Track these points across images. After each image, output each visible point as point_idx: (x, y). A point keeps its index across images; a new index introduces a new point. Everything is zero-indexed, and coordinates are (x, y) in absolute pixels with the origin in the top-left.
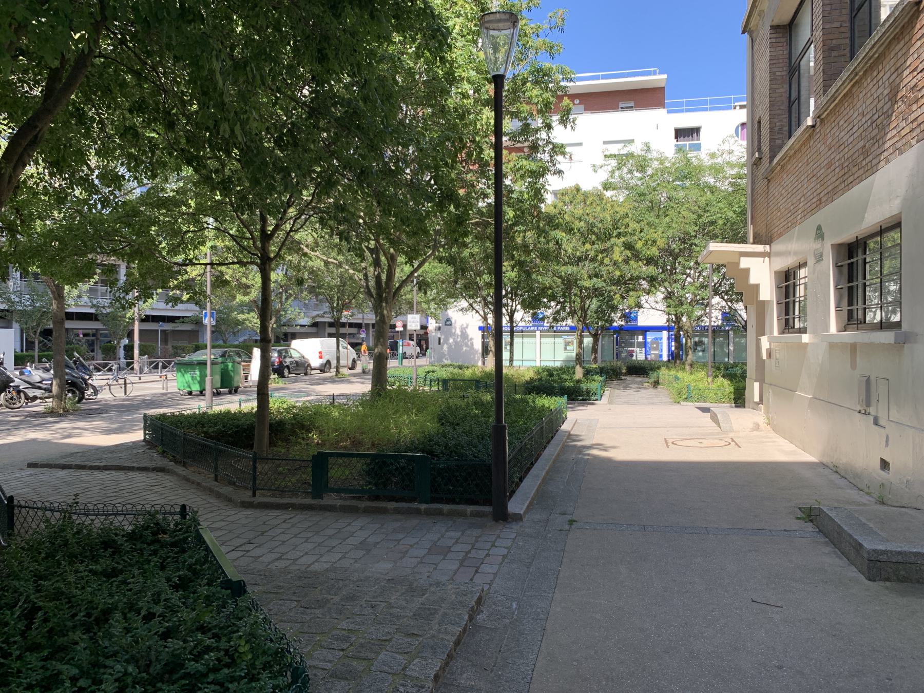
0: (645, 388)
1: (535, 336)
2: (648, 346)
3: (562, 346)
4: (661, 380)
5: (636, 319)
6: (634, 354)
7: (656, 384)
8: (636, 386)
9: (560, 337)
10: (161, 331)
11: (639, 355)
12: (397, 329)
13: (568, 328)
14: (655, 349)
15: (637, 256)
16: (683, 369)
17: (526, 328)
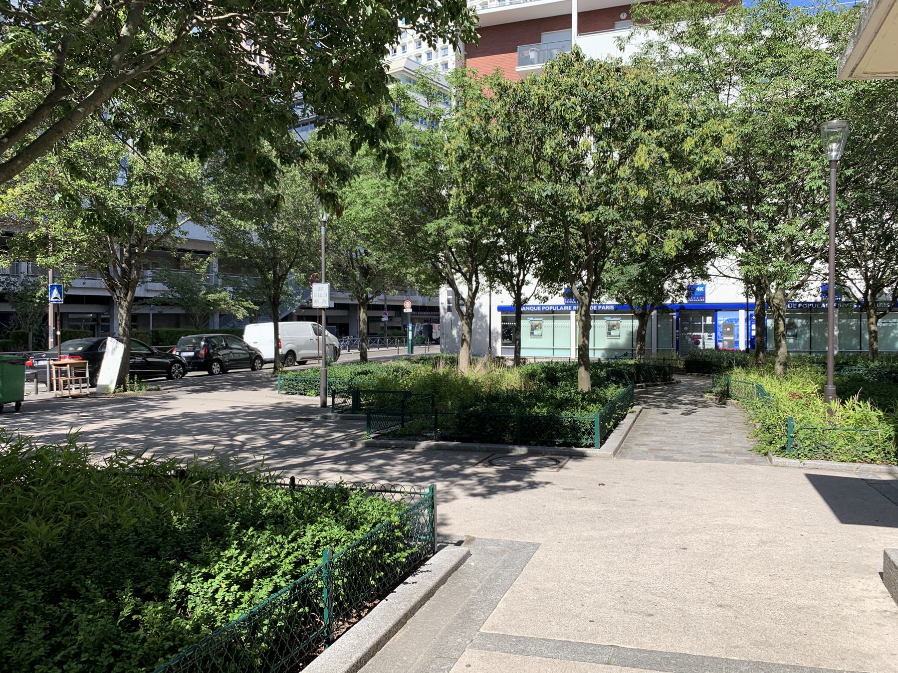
0: (705, 405)
1: (569, 318)
2: (720, 329)
3: (605, 330)
4: (733, 391)
5: (703, 295)
6: (701, 340)
7: (724, 396)
8: (691, 398)
9: (602, 318)
10: (153, 314)
11: (708, 342)
12: (405, 311)
13: (612, 308)
14: (730, 333)
15: (679, 160)
16: (771, 371)
17: (557, 308)
